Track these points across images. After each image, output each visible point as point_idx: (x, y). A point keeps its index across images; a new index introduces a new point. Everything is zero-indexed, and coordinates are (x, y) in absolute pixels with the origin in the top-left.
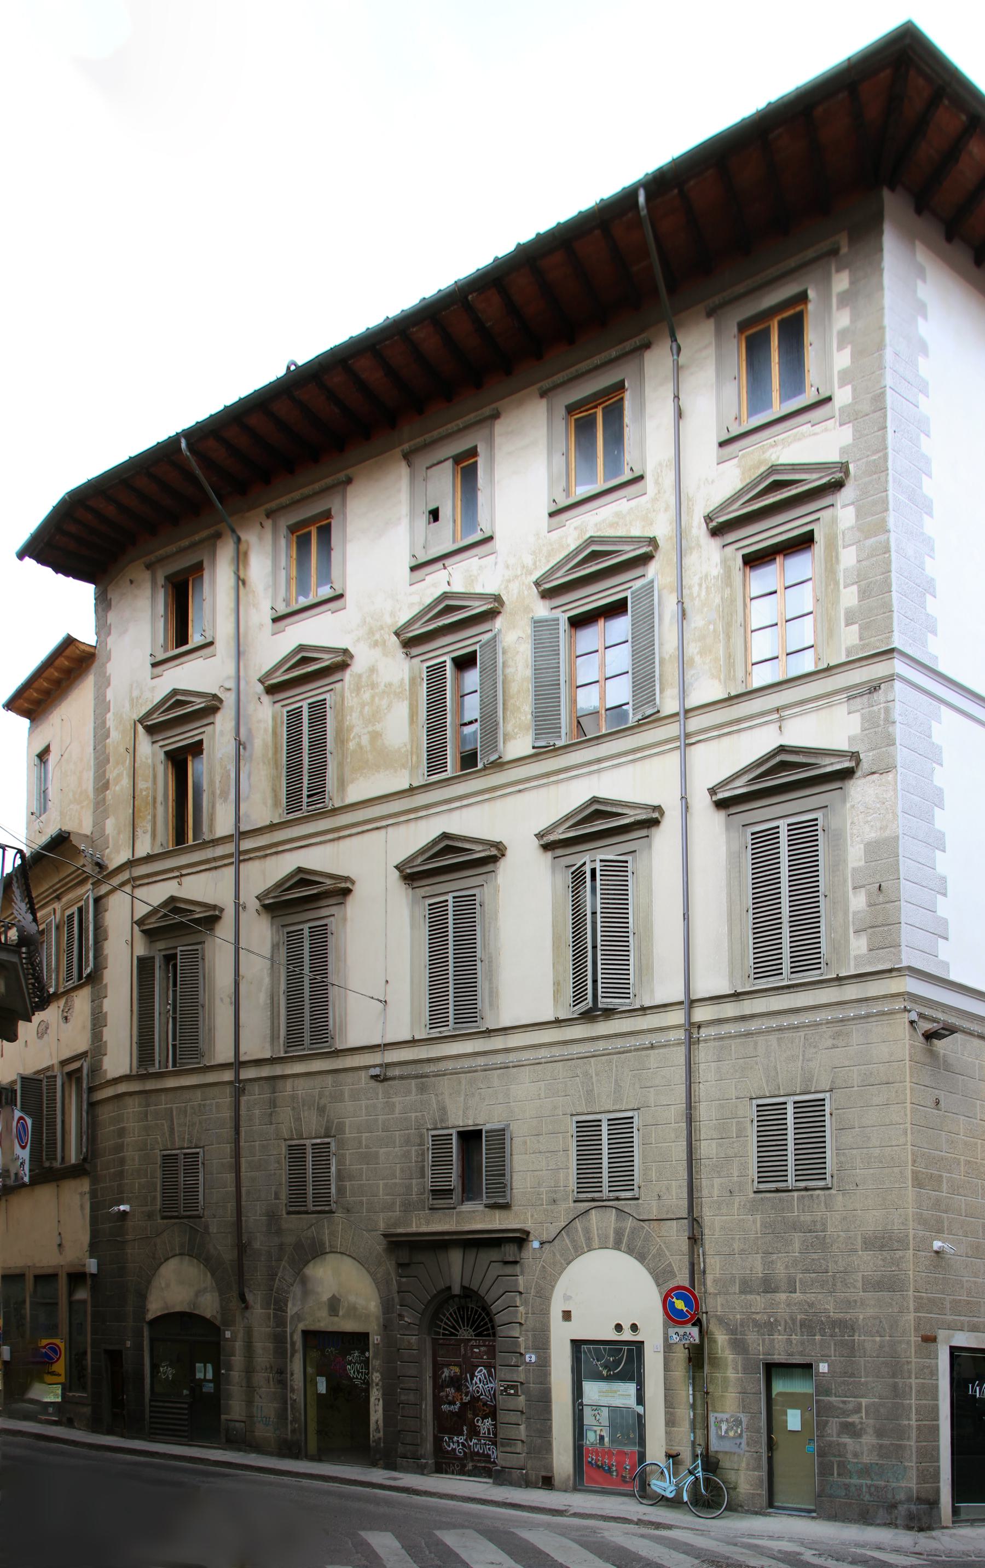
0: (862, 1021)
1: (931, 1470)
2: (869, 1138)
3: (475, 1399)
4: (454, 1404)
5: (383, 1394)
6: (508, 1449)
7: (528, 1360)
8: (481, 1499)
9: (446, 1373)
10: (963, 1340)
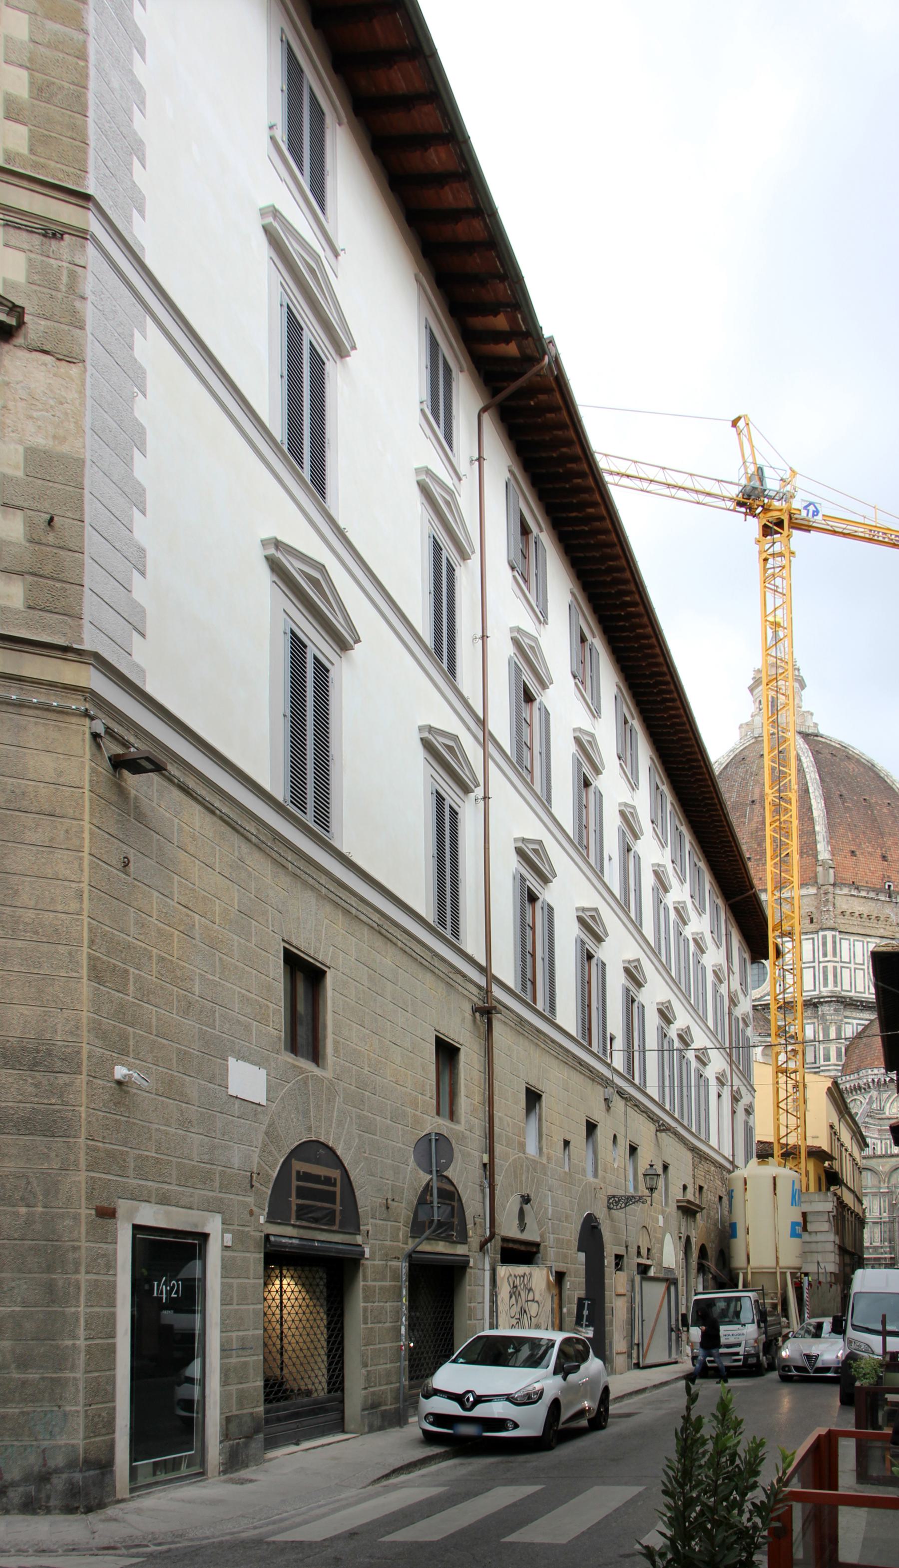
0: (11, 709)
1: (104, 1414)
2: (16, 893)
10: (151, 1215)
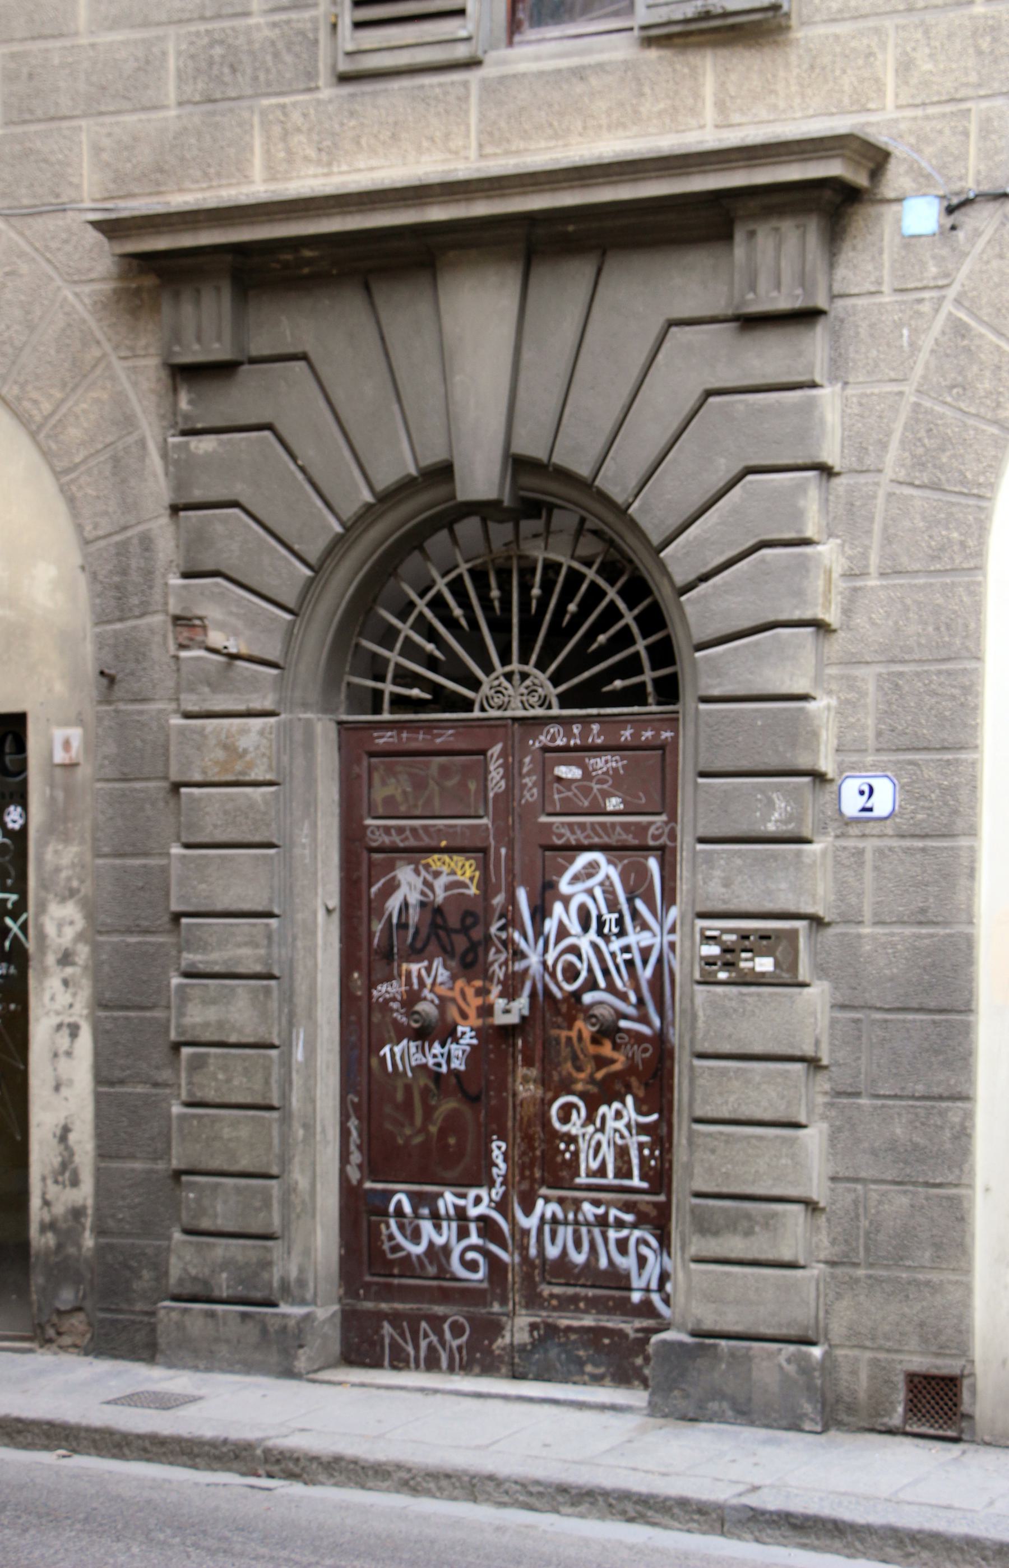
3: (554, 1010)
4: (450, 1034)
5: (100, 1003)
6: (735, 1246)
7: (851, 804)
8: (626, 1496)
9: (409, 887)
